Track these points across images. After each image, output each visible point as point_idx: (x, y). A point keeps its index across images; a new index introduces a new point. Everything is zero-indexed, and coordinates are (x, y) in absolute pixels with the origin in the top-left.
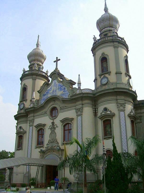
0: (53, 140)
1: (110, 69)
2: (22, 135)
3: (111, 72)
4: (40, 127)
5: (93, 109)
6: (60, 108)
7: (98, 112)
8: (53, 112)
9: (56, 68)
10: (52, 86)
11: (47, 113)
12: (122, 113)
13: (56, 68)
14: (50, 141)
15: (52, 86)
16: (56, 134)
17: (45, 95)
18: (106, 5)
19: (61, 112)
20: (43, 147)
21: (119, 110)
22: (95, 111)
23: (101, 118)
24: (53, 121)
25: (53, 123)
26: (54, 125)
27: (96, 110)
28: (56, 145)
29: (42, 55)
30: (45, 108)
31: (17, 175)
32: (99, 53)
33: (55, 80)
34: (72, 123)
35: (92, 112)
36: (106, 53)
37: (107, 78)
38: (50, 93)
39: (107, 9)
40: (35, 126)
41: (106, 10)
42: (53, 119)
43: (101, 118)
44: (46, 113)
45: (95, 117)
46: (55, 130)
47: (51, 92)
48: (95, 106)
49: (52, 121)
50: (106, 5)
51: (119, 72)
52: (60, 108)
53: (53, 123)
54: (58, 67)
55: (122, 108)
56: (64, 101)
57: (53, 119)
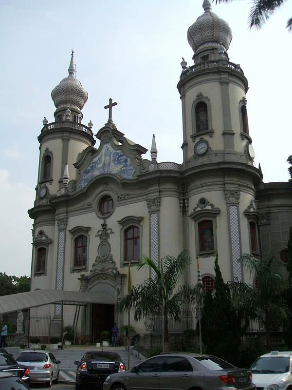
0: (105, 258)
5: (180, 200)
6: (118, 197)
7: (188, 206)
8: (105, 205)
9: (110, 121)
13: (110, 121)
17: (89, 171)
22: (184, 203)
27: (185, 201)
37: (206, 142)
38: (98, 169)
41: (71, 71)
42: (105, 219)
44: (90, 206)
47: (100, 166)
49: (102, 222)
52: (118, 197)
53: (104, 226)
54: (113, 118)
56: (125, 184)
57: (105, 219)
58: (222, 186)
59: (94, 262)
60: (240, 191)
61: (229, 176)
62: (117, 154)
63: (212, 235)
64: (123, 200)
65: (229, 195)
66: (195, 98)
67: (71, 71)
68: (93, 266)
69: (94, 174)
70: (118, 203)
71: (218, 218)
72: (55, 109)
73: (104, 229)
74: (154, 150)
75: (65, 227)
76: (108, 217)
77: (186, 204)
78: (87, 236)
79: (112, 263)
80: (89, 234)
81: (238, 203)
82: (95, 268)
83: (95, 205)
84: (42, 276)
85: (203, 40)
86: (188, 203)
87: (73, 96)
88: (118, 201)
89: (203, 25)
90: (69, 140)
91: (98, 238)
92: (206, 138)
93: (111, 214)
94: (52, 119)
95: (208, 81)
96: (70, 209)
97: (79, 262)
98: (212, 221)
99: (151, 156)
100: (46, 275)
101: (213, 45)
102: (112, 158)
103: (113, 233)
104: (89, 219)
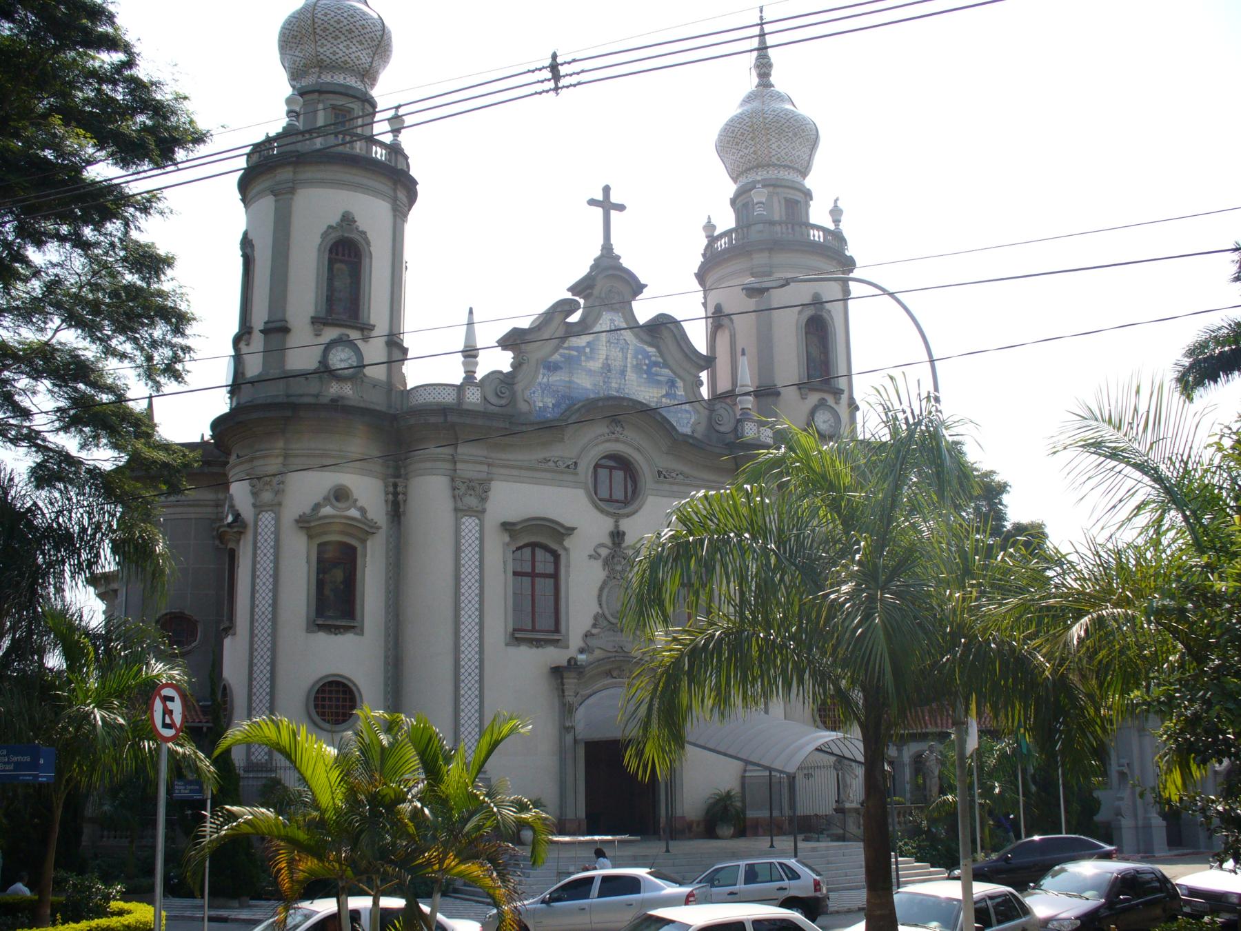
1: (372, 316)
2: (354, 542)
3: (308, 320)
8: (620, 483)
9: (607, 247)
11: (576, 474)
12: (469, 524)
13: (607, 247)
14: (605, 623)
17: (555, 367)
21: (456, 510)
22: (396, 494)
24: (617, 526)
25: (617, 536)
27: (399, 489)
29: (363, 27)
30: (562, 440)
31: (808, 776)
35: (382, 497)
36: (362, 224)
38: (590, 372)
40: (507, 527)
42: (617, 517)
47: (595, 365)
49: (607, 524)
52: (659, 473)
53: (617, 536)
54: (614, 240)
55: (472, 501)
56: (680, 444)
57: (617, 517)
62: (647, 356)
63: (320, 584)
72: (731, 188)
76: (628, 515)
77: (400, 497)
78: (561, 552)
80: (566, 543)
81: (484, 511)
83: (586, 467)
84: (349, 638)
85: (791, 161)
87: (348, 47)
88: (657, 482)
90: (292, 191)
91: (598, 564)
94: (726, 220)
97: (537, 622)
100: (361, 633)
101: (768, 176)
102: (630, 361)
104: (567, 503)
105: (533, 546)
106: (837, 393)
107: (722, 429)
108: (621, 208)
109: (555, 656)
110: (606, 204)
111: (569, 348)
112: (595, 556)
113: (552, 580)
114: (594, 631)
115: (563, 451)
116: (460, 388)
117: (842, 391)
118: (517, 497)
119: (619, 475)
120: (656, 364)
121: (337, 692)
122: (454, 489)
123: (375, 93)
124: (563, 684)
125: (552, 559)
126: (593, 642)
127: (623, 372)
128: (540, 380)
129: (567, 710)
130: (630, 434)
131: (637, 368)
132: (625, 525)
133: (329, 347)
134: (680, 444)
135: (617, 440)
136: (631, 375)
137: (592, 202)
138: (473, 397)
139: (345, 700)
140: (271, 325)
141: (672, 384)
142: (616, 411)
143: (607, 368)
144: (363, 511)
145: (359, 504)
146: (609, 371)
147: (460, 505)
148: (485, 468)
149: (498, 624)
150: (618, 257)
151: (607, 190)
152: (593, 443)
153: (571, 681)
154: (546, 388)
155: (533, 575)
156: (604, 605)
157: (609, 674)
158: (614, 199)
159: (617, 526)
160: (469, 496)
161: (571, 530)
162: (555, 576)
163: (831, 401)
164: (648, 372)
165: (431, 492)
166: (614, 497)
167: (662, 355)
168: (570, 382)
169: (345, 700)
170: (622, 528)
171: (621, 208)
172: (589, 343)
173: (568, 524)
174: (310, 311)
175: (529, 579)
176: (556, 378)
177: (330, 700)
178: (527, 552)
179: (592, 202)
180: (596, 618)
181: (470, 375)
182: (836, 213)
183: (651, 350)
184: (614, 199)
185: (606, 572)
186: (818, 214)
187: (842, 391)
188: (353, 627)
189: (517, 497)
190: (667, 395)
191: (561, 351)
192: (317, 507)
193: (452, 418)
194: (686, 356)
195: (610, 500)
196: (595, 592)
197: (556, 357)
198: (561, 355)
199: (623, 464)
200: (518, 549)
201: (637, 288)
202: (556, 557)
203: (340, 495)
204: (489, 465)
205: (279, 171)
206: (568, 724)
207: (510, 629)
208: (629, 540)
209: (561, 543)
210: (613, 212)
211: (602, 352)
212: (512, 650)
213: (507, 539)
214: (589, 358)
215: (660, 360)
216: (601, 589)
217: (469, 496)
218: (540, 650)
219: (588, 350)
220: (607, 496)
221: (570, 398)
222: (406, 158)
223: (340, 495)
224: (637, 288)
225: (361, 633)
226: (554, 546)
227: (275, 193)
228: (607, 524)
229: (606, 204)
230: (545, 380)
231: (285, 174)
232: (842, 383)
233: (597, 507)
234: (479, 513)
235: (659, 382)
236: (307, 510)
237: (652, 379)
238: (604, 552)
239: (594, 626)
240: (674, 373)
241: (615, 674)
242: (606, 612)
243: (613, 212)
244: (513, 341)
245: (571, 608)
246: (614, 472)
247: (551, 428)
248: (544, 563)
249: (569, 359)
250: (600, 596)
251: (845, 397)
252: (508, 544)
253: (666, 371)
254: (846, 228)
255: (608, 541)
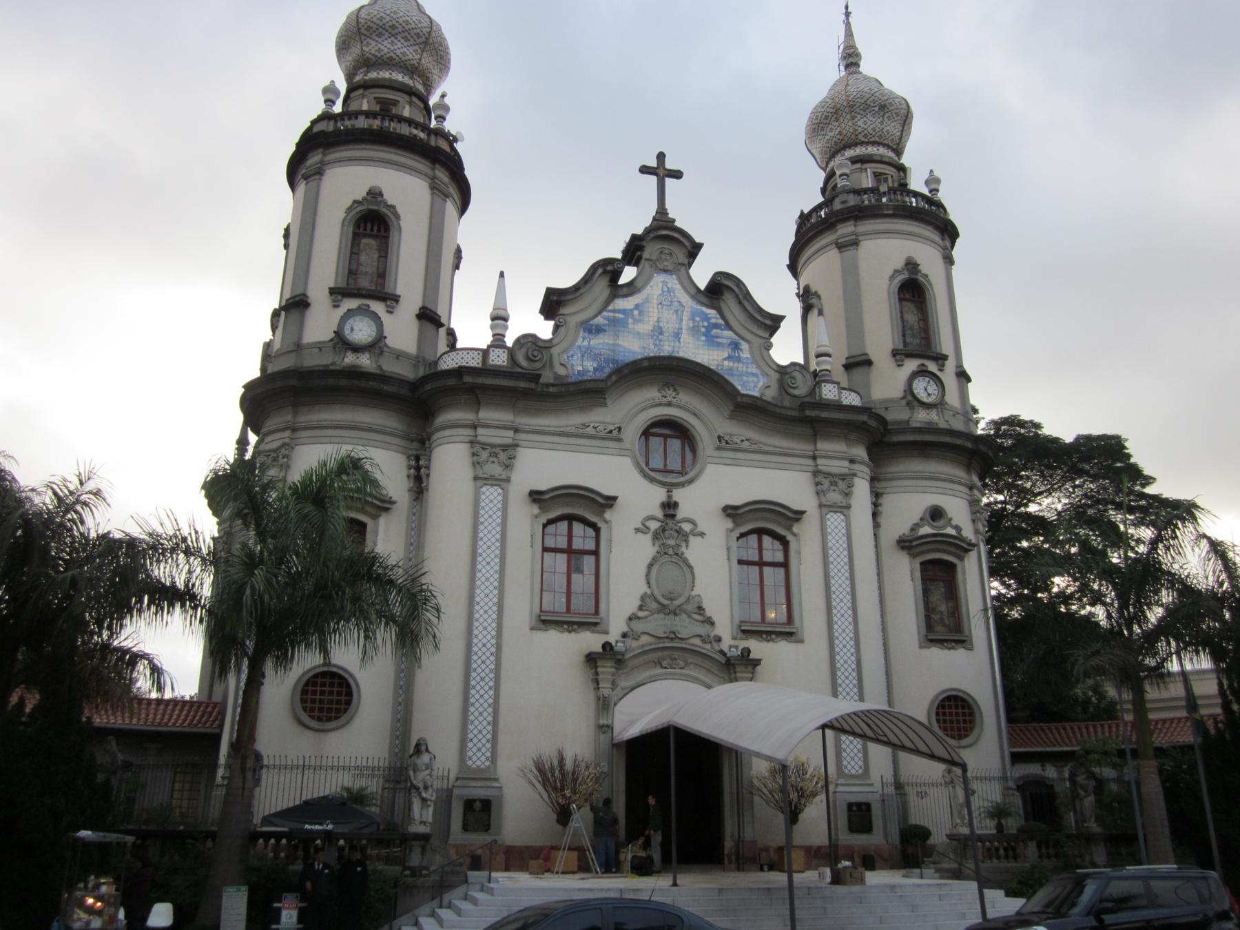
0: (669, 601)
2: (363, 518)
4: (757, 520)
5: (408, 457)
6: (720, 438)
7: (428, 475)
9: (662, 211)
10: (647, 300)
11: (620, 440)
12: (491, 494)
13: (662, 211)
14: (654, 605)
15: (647, 300)
16: (690, 567)
17: (599, 330)
18: (849, 34)
19: (715, 460)
20: (598, 628)
23: (906, 544)
24: (670, 497)
25: (670, 507)
26: (679, 517)
27: (421, 462)
28: (702, 630)
30: (605, 405)
32: (348, 181)
33: (665, 271)
34: (607, 522)
35: (405, 472)
37: (375, 317)
39: (858, 55)
40: (536, 496)
41: (851, 59)
42: (670, 487)
43: (906, 544)
44: (613, 435)
45: (416, 499)
46: (684, 549)
47: (646, 327)
48: (422, 442)
49: (660, 494)
50: (849, 34)
51: (859, 359)
52: (720, 438)
53: (670, 507)
54: (669, 205)
56: (748, 409)
57: (670, 487)
58: (810, 462)
59: (632, 605)
60: (855, 475)
61: (828, 437)
64: (735, 450)
65: (826, 483)
66: (360, 194)
67: (851, 59)
68: (630, 619)
69: (620, 342)
70: (717, 453)
71: (382, 521)
73: (666, 516)
74: (501, 313)
75: (282, 474)
76: (682, 485)
78: (789, 537)
79: (703, 622)
80: (795, 529)
81: (848, 507)
82: (638, 626)
83: (632, 433)
86: (428, 467)
88: (719, 449)
89: (891, 104)
90: (855, 243)
91: (647, 538)
92: (377, 307)
93: (691, 481)
95: (351, 160)
96: (306, 418)
98: (364, 525)
99: (492, 327)
102: (686, 323)
103: (702, 534)
105: (760, 532)
106: (941, 359)
107: (796, 392)
108: (677, 175)
109: (592, 641)
110: (661, 171)
111: (614, 311)
112: (642, 529)
113: (781, 571)
114: (641, 614)
115: (600, 417)
116: (485, 353)
117: (945, 358)
118: (546, 464)
119: (675, 444)
120: (716, 326)
121: (332, 685)
122: (817, 484)
123: (905, 160)
124: (597, 674)
125: (781, 547)
126: (638, 626)
127: (677, 335)
128: (579, 342)
129: (604, 705)
130: (685, 397)
131: (695, 330)
132: (679, 495)
133: (350, 313)
134: (748, 409)
135: (669, 404)
136: (686, 337)
137: (645, 170)
138: (499, 359)
139: (339, 694)
140: (851, 361)
141: (736, 346)
142: (668, 371)
143: (659, 331)
144: (958, 528)
145: (954, 523)
146: (661, 333)
147: (824, 501)
148: (510, 433)
149: (520, 608)
150: (674, 221)
151: (661, 157)
152: (636, 407)
153: (606, 669)
154: (587, 352)
155: (761, 564)
156: (653, 582)
157: (658, 663)
158: (670, 164)
159: (670, 497)
160: (493, 463)
161: (610, 501)
162: (785, 565)
163: (932, 367)
164: (707, 334)
165: (451, 459)
166: (669, 468)
167: (723, 317)
168: (615, 345)
169: (339, 694)
170: (675, 498)
171: (677, 175)
172: (637, 307)
173: (796, 507)
174: (889, 347)
175: (757, 568)
176: (598, 342)
177: (951, 714)
178: (754, 538)
179: (645, 170)
180: (643, 598)
181: (498, 341)
182: (933, 181)
183: (711, 312)
184: (670, 164)
185: (656, 548)
186: (917, 183)
187: (945, 358)
188: (791, 634)
189: (546, 464)
190: (729, 358)
191: (605, 314)
192: (914, 528)
193: (468, 379)
194: (751, 317)
195: (666, 471)
196: (643, 570)
197: (599, 320)
198: (605, 318)
199: (676, 430)
200: (742, 535)
201: (694, 249)
202: (597, 530)
203: (936, 514)
204: (516, 430)
205: (839, 226)
206: (603, 721)
207: (737, 622)
208: (681, 513)
209: (789, 529)
210: (668, 181)
211: (653, 314)
212: (926, 652)
213: (730, 524)
214: (636, 321)
215: (721, 322)
216: (650, 566)
217: (493, 463)
218: (573, 635)
219: (636, 312)
220: (661, 466)
221: (614, 361)
222: (945, 210)
223: (936, 514)
224: (694, 249)
225: (970, 648)
226: (781, 531)
227: (841, 247)
228: (660, 494)
229: (661, 171)
230: (585, 343)
231: (846, 229)
232: (946, 347)
233: (645, 476)
234: (502, 482)
235: (719, 345)
236: (907, 532)
237: (711, 341)
238: (654, 525)
239: (641, 608)
240: (736, 333)
241: (665, 663)
242: (656, 593)
243: (668, 181)
244: (553, 304)
245: (612, 587)
246: (669, 441)
247: (588, 393)
248: (772, 550)
249: (614, 322)
250: (648, 575)
251: (950, 365)
252: (731, 531)
253: (729, 333)
254: (943, 196)
255: (659, 514)
